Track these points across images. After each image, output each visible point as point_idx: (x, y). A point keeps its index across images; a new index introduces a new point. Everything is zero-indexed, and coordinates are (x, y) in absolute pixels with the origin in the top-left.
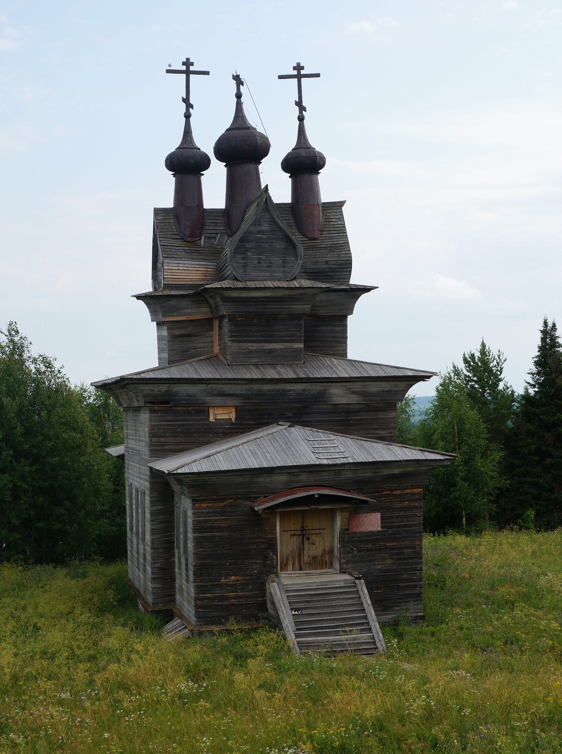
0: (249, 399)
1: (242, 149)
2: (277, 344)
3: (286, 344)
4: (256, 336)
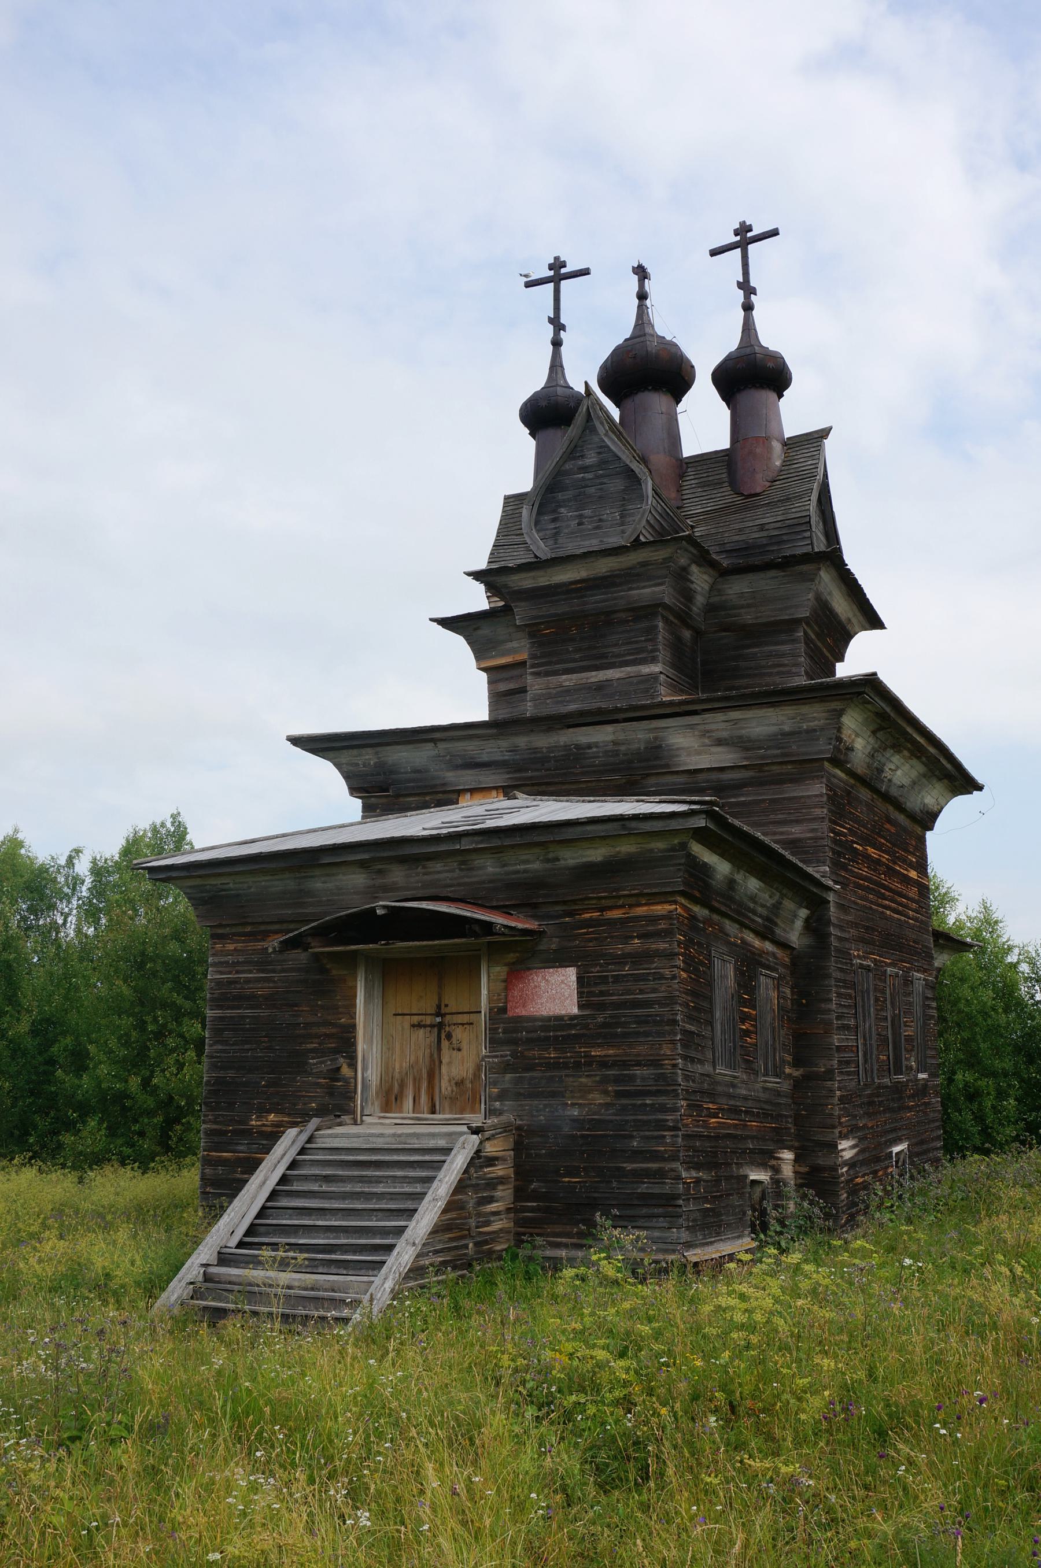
0: (519, 771)
1: (647, 371)
2: (611, 671)
3: (629, 669)
4: (575, 661)
